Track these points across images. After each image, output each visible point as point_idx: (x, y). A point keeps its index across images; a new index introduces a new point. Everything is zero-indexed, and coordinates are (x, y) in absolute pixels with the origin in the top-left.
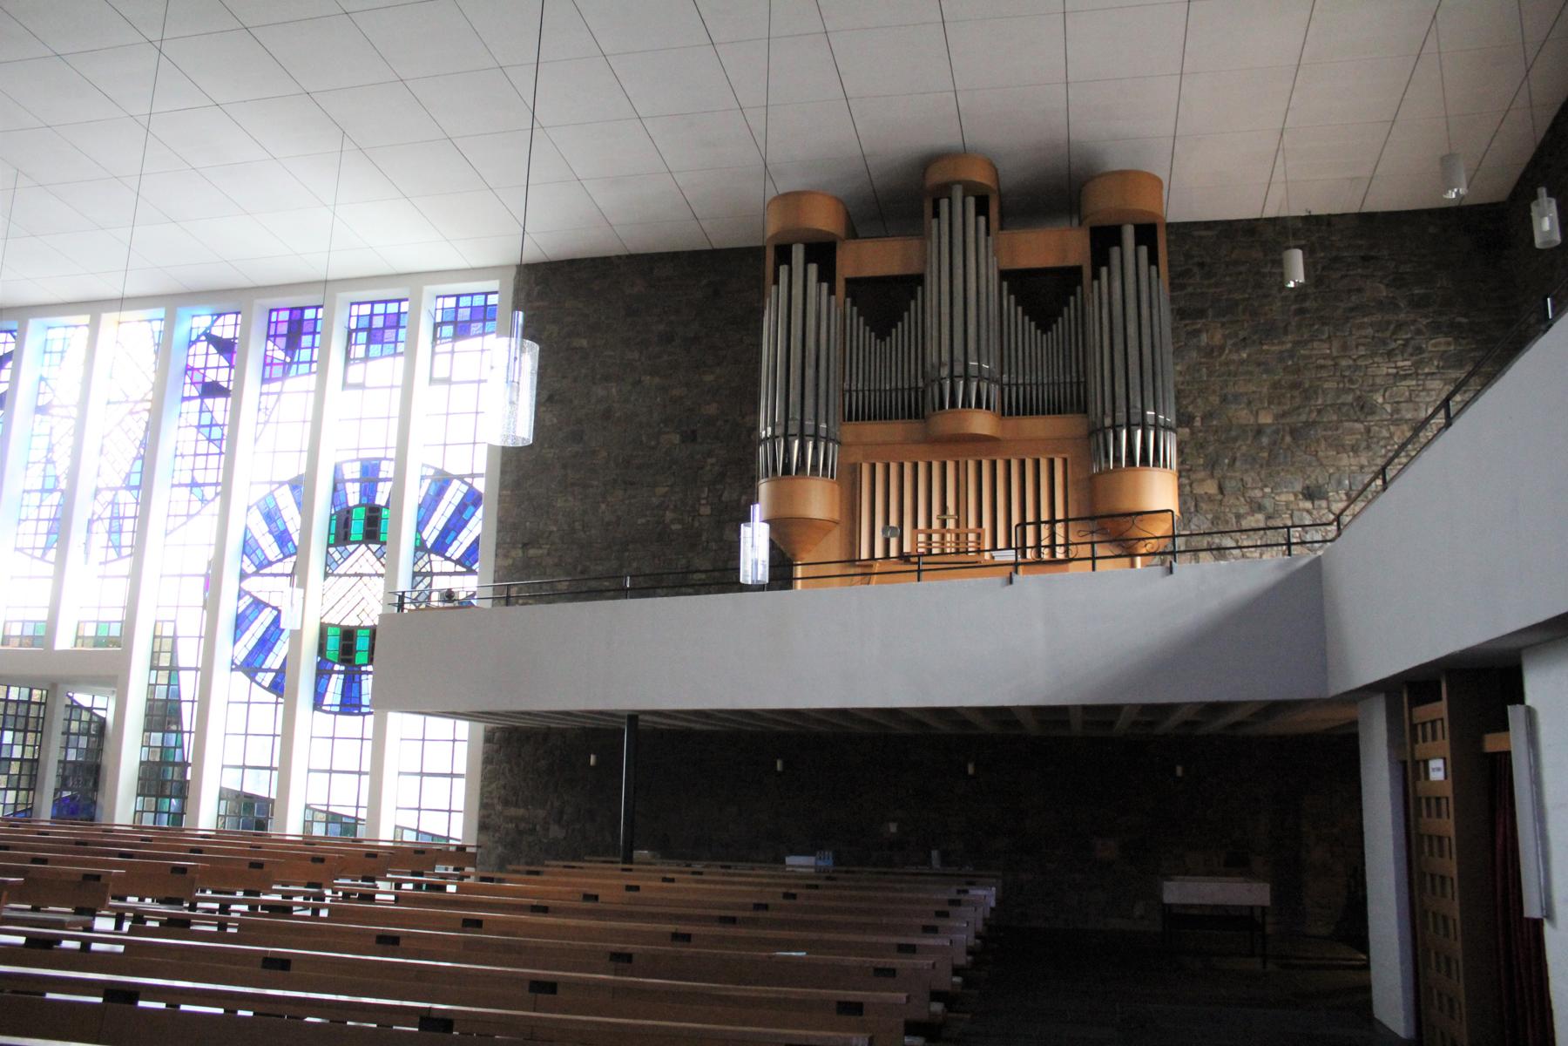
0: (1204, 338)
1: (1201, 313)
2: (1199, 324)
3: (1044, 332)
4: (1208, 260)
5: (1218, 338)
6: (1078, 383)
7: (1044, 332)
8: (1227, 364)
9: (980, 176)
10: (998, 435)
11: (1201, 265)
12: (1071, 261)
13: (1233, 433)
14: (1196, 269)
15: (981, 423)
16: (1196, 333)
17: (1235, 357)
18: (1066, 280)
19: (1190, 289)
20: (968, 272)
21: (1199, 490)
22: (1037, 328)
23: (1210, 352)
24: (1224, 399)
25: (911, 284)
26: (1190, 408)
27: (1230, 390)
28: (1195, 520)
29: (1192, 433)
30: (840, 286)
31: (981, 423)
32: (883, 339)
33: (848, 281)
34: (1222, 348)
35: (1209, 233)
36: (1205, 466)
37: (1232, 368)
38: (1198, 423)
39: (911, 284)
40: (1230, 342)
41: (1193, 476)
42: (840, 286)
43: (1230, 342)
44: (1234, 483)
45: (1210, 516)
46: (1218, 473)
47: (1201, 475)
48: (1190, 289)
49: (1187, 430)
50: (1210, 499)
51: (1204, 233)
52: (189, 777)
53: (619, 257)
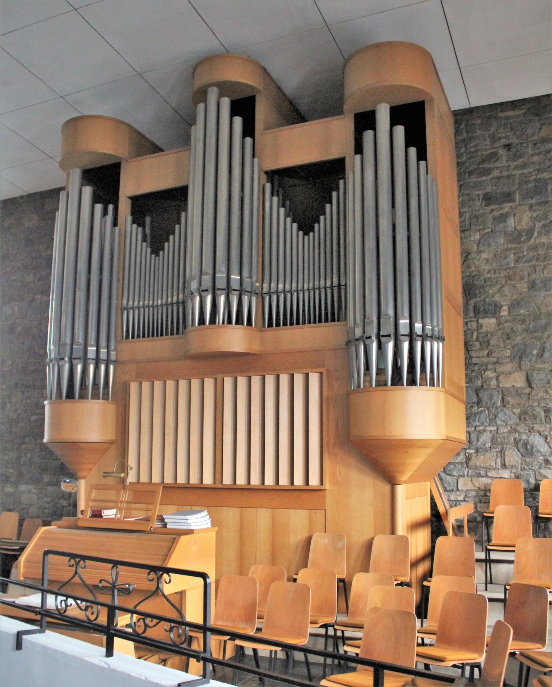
0: (511, 222)
1: (508, 197)
2: (507, 207)
3: (306, 233)
4: (515, 141)
5: (525, 221)
6: (339, 285)
7: (306, 233)
8: (535, 248)
9: (241, 76)
10: (256, 348)
11: (508, 146)
12: (334, 155)
13: (543, 322)
14: (502, 152)
15: (234, 339)
16: (503, 218)
17: (544, 240)
18: (325, 176)
19: (496, 173)
20: (222, 178)
21: (506, 383)
22: (299, 229)
23: (516, 237)
24: (532, 286)
25: (178, 196)
26: (497, 298)
27: (538, 277)
28: (501, 415)
29: (499, 324)
30: (125, 206)
31: (234, 339)
32: (157, 255)
33: (136, 200)
34: (530, 232)
35: (516, 112)
36: (512, 358)
37: (541, 252)
38: (504, 312)
39: (178, 196)
40: (538, 225)
41: (500, 369)
42: (125, 206)
43: (538, 225)
44: (542, 376)
45: (517, 411)
46: (526, 364)
47: (508, 367)
48: (496, 173)
49: (493, 320)
50: (518, 392)
51: (511, 113)
52: (18, 548)
53: (22, 197)
